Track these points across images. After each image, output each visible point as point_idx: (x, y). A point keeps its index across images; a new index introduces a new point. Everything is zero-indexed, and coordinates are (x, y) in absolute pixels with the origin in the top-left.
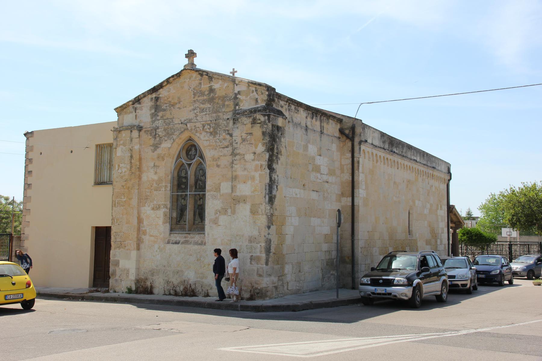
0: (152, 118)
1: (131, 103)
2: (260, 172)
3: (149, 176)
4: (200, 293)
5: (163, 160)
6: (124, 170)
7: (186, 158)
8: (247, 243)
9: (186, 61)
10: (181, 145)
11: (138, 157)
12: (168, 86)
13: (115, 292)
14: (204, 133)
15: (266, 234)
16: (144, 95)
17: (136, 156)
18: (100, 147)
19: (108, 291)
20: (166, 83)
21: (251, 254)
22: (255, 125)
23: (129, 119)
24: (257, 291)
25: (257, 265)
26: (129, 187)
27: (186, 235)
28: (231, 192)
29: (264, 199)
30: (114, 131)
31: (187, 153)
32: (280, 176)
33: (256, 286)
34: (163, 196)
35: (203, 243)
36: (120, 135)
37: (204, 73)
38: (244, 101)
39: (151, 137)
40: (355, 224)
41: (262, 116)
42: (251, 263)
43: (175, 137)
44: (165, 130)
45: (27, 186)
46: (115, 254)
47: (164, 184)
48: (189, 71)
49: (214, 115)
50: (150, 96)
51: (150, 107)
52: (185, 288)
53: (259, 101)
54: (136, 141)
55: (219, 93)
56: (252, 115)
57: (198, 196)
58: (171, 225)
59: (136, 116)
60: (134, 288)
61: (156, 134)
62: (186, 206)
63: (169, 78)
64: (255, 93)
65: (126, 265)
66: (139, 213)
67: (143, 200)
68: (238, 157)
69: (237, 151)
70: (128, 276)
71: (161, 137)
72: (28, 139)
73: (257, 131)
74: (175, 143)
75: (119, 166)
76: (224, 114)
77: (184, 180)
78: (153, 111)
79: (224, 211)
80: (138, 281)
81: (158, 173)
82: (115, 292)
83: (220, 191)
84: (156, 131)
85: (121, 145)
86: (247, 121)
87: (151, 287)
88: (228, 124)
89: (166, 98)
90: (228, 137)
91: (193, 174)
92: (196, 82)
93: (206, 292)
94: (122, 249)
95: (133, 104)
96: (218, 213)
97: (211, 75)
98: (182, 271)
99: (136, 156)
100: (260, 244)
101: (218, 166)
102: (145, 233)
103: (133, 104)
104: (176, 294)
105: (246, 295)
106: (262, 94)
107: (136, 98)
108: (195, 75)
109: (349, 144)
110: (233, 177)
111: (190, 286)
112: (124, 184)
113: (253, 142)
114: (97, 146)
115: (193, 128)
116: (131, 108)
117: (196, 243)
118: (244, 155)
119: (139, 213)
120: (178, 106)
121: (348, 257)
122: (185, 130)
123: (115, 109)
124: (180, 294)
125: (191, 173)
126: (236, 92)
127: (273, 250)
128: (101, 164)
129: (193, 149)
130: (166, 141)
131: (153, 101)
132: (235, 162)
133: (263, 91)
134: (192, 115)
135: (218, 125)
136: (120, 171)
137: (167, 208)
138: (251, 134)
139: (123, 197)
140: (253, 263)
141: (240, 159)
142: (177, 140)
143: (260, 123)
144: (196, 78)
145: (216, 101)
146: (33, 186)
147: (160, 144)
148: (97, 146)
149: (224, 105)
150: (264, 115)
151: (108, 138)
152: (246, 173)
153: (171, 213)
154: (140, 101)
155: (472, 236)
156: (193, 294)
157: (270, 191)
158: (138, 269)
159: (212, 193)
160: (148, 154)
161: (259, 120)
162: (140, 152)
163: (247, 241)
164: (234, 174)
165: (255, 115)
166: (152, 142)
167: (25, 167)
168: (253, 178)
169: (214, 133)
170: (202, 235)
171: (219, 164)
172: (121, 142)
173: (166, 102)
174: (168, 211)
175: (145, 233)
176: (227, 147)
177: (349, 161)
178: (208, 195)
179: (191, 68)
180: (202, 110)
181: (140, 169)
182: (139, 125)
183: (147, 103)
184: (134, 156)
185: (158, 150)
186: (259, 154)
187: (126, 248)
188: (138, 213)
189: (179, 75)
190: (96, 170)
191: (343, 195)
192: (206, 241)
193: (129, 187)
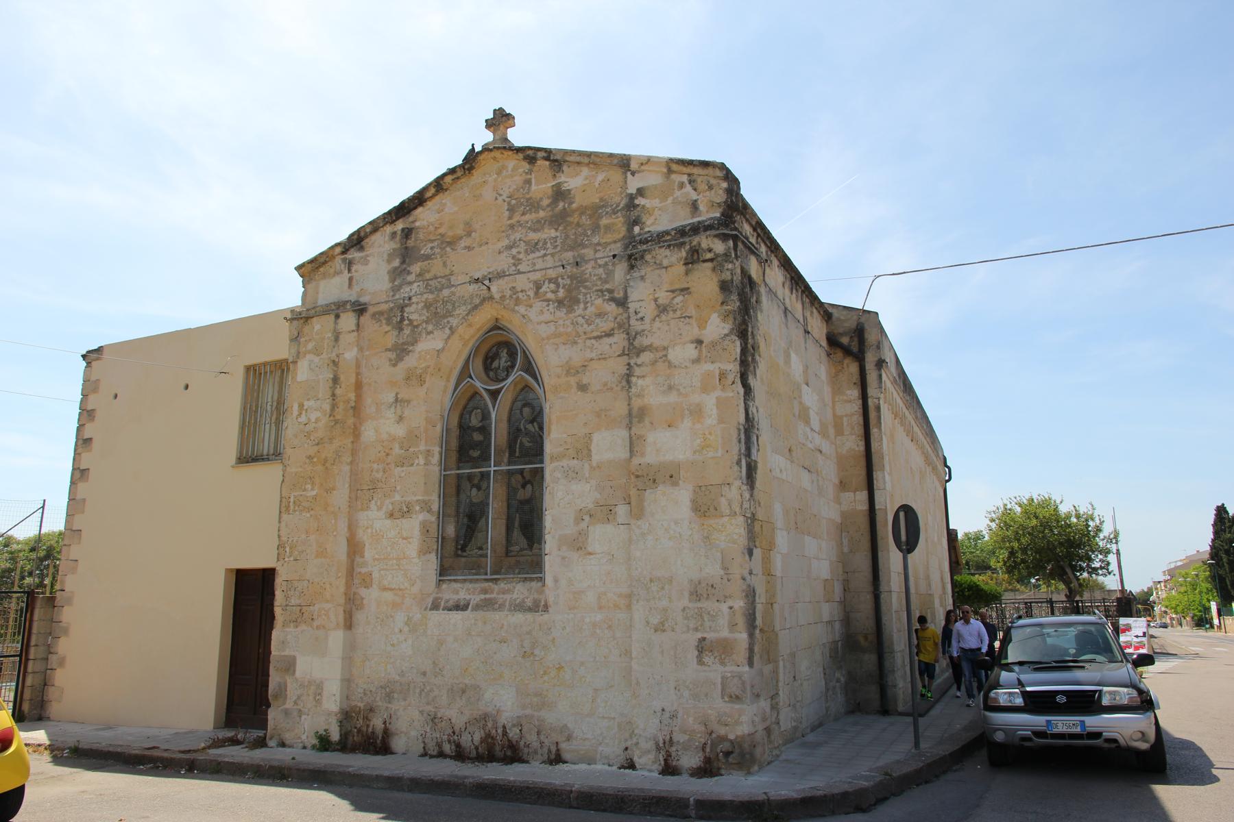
0: (393, 280)
1: (338, 250)
2: (718, 393)
3: (383, 427)
4: (536, 752)
5: (422, 381)
6: (313, 417)
7: (483, 375)
8: (685, 602)
10: (470, 345)
11: (353, 380)
12: (437, 198)
13: (283, 744)
14: (538, 305)
15: (746, 573)
16: (374, 226)
17: (348, 379)
18: (255, 373)
19: (261, 743)
20: (433, 190)
21: (700, 635)
22: (695, 266)
23: (333, 288)
24: (726, 746)
25: (721, 668)
26: (326, 460)
27: (486, 585)
29: (736, 468)
30: (292, 320)
31: (487, 367)
32: (761, 410)
33: (722, 731)
34: (420, 479)
35: (539, 607)
36: (306, 329)
37: (540, 154)
38: (657, 212)
39: (389, 328)
40: (880, 554)
41: (716, 241)
42: (700, 662)
43: (454, 322)
44: (427, 306)
45: (78, 474)
46: (285, 639)
47: (422, 448)
48: (497, 154)
49: (569, 255)
50: (389, 229)
52: (488, 735)
53: (702, 207)
54: (348, 339)
55: (579, 201)
56: (687, 239)
57: (519, 477)
58: (442, 559)
59: (351, 279)
60: (335, 736)
62: (484, 505)
63: (444, 175)
64: (688, 188)
65: (314, 672)
66: (352, 528)
67: (363, 491)
68: (646, 357)
69: (641, 341)
70: (318, 702)
71: (417, 327)
72: (89, 364)
73: (705, 282)
74: (456, 336)
75: (301, 406)
76: (596, 251)
77: (477, 437)
78: (396, 263)
79: (605, 513)
80: (346, 716)
81: (408, 418)
82: (283, 744)
85: (310, 352)
86: (673, 258)
87: (387, 733)
88: (610, 274)
90: (611, 308)
91: (505, 417)
93: (554, 749)
94: (303, 627)
95: (343, 253)
96: (587, 518)
97: (558, 157)
98: (476, 687)
99: (348, 379)
100: (730, 603)
101: (583, 388)
102: (367, 582)
103: (343, 253)
104: (460, 755)
105: (689, 760)
106: (710, 188)
107: (352, 235)
108: (512, 162)
109: (853, 368)
110: (635, 412)
111: (505, 733)
112: (312, 451)
113: (692, 311)
114: (248, 368)
115: (508, 293)
116: (338, 263)
117: (519, 607)
118: (665, 348)
119: (352, 528)
120: (463, 243)
121: (866, 638)
122: (483, 300)
123: (298, 268)
124: (474, 754)
125: (498, 415)
126: (632, 190)
127: (759, 622)
128: (256, 412)
130: (429, 333)
132: (638, 371)
133: (713, 181)
134: (504, 262)
135: (579, 281)
136: (303, 419)
137: (430, 511)
138: (685, 290)
139: (309, 486)
140: (706, 659)
141: (654, 363)
142: (461, 330)
143: (711, 260)
144: (515, 169)
145: (574, 219)
146: (92, 474)
147: (415, 342)
148: (248, 368)
150: (724, 238)
151: (282, 351)
152: (673, 398)
153: (441, 525)
155: (963, 591)
156: (513, 754)
157: (748, 454)
158: (347, 681)
159: (565, 462)
160: (381, 371)
161: (710, 250)
162: (358, 366)
163: (686, 594)
164: (637, 403)
165: (696, 240)
166: (391, 338)
167: (78, 429)
168: (697, 412)
169: (568, 302)
170: (534, 584)
172: (310, 346)
174: (434, 519)
175: (367, 582)
176: (609, 334)
177: (856, 407)
178: (552, 470)
180: (534, 247)
181: (357, 410)
183: (382, 244)
184: (342, 378)
185: (406, 358)
186: (714, 344)
187: (315, 624)
190: (242, 428)
191: (843, 485)
192: (551, 600)
193: (326, 460)
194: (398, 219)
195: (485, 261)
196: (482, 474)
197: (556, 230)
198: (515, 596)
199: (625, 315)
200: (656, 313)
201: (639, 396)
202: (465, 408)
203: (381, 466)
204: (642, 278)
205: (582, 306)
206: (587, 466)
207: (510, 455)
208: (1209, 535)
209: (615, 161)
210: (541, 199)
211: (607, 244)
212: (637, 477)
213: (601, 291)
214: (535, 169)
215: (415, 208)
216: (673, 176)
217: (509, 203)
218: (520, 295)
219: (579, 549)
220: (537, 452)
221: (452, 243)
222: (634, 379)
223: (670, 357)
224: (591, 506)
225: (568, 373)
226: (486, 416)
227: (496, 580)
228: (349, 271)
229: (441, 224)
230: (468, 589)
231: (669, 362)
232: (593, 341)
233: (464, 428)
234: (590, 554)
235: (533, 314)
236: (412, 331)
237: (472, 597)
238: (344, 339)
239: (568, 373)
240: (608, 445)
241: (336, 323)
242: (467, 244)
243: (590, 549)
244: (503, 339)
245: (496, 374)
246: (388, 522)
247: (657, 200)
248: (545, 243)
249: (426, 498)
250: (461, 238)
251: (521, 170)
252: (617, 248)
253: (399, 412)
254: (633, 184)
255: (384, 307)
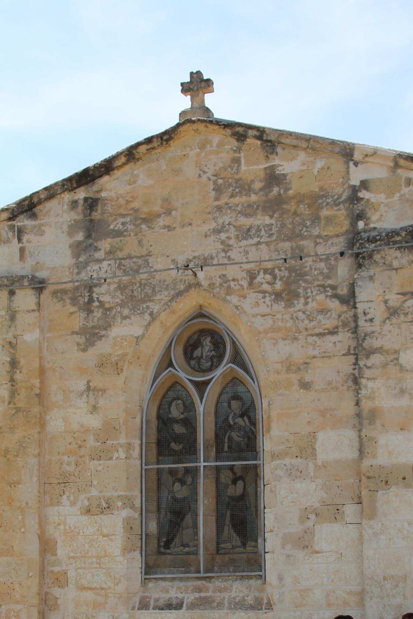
0: (77, 256)
3: (71, 417)
5: (118, 369)
9: (185, 102)
11: (36, 365)
12: (127, 168)
14: (253, 296)
16: (51, 192)
20: (123, 159)
27: (199, 583)
28: (355, 454)
34: (121, 472)
37: (251, 133)
38: (382, 208)
39: (74, 309)
43: (155, 308)
44: (122, 288)
47: (123, 440)
48: (201, 127)
49: (287, 245)
50: (67, 197)
51: (71, 227)
57: (230, 474)
59: (22, 250)
61: (91, 300)
63: (139, 144)
66: (42, 524)
67: (54, 485)
68: (376, 359)
74: (157, 323)
76: (316, 244)
77: (179, 429)
78: (80, 236)
79: (335, 513)
83: (314, 454)
84: (91, 291)
88: (332, 269)
89: (121, 201)
90: (335, 305)
92: (223, 155)
95: (10, 219)
96: (313, 517)
97: (272, 138)
101: (305, 386)
102: (61, 580)
103: (10, 219)
107: (24, 200)
108: (217, 137)
110: (365, 413)
117: (239, 605)
119: (42, 524)
120: (162, 221)
125: (204, 410)
126: (355, 181)
129: (207, 342)
130: (125, 318)
131: (80, 208)
132: (367, 373)
134: (211, 247)
137: (132, 507)
141: (385, 365)
142: (163, 316)
145: (292, 206)
147: (108, 326)
148: (192, 74)
149: (316, 219)
154: (35, 210)
159: (287, 461)
160: (67, 353)
169: (287, 295)
170: (253, 582)
171: (307, 379)
173: (122, 211)
174: (137, 515)
175: (61, 580)
176: (333, 332)
178: (270, 469)
179: (198, 119)
180: (246, 233)
182: (33, 277)
183: (60, 215)
184: (22, 362)
185: (99, 344)
188: (41, 525)
189: (166, 137)
192: (275, 598)
194: (78, 186)
195: (190, 243)
196: (187, 471)
197: (271, 217)
198: (233, 594)
199: (351, 313)
200: (386, 315)
201: (370, 398)
202: (164, 397)
203: (73, 459)
204: (371, 278)
205: (302, 300)
206: (311, 465)
207: (218, 452)
208: (205, 98)
209: (337, 150)
210: (252, 181)
211: (328, 238)
212: (369, 478)
213: (323, 286)
214: (244, 147)
215: (101, 176)
216: (399, 171)
217: (215, 183)
218: (232, 284)
219: (305, 547)
220: (249, 446)
221: (149, 220)
222: (364, 381)
223: (401, 360)
224: (317, 505)
225: (289, 370)
226: (189, 407)
227: (210, 578)
228: (20, 240)
229: (134, 198)
230: (178, 588)
231: (401, 366)
232: (315, 338)
233: (164, 421)
234: (317, 552)
235: (247, 305)
236: (104, 314)
237: (186, 596)
238: (22, 319)
239: (289, 370)
240: (335, 445)
241: (10, 301)
242: (167, 224)
243: (316, 548)
244: (210, 327)
245: (199, 363)
246: (84, 519)
247: (383, 196)
248: (259, 230)
249: (129, 494)
250: (159, 216)
251: (228, 147)
252: (339, 244)
253: (92, 401)
254: (357, 176)
255: (70, 286)
